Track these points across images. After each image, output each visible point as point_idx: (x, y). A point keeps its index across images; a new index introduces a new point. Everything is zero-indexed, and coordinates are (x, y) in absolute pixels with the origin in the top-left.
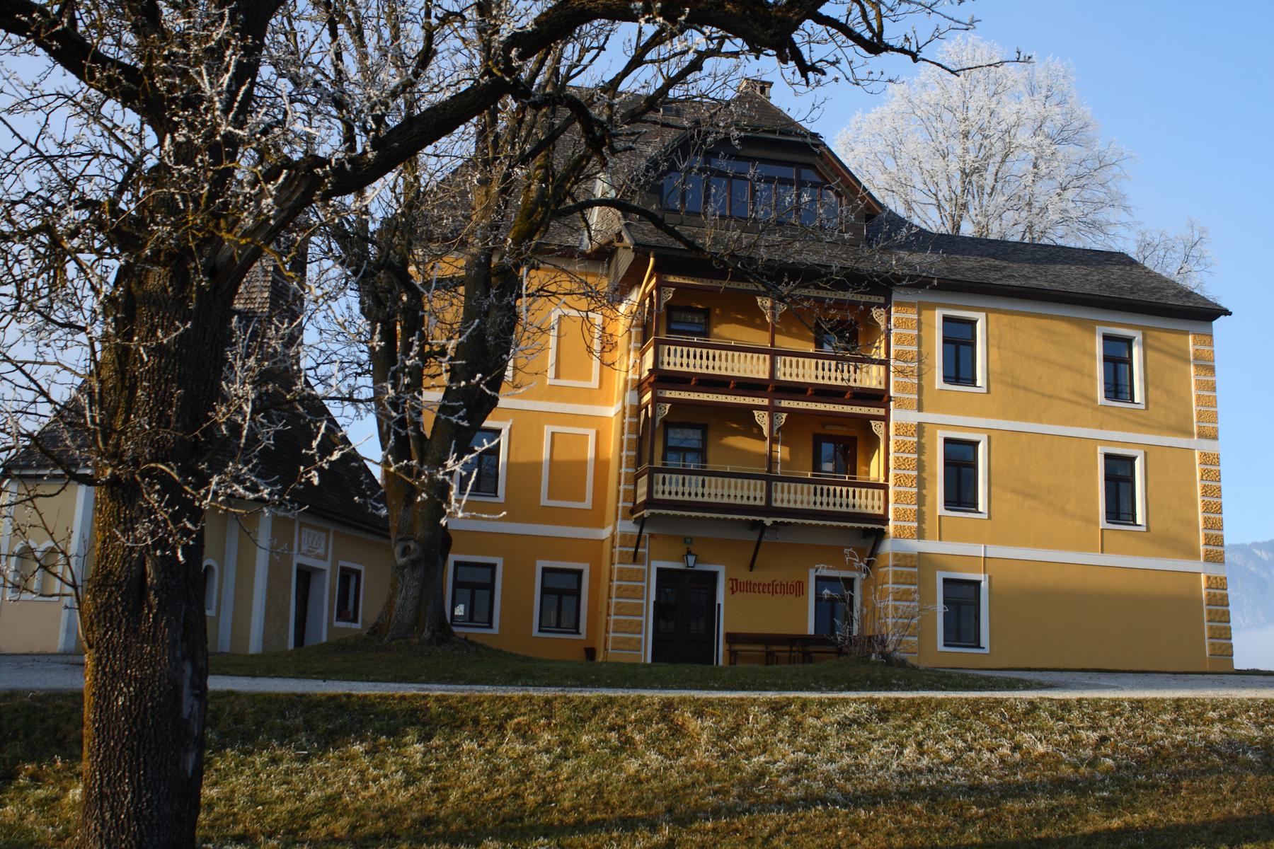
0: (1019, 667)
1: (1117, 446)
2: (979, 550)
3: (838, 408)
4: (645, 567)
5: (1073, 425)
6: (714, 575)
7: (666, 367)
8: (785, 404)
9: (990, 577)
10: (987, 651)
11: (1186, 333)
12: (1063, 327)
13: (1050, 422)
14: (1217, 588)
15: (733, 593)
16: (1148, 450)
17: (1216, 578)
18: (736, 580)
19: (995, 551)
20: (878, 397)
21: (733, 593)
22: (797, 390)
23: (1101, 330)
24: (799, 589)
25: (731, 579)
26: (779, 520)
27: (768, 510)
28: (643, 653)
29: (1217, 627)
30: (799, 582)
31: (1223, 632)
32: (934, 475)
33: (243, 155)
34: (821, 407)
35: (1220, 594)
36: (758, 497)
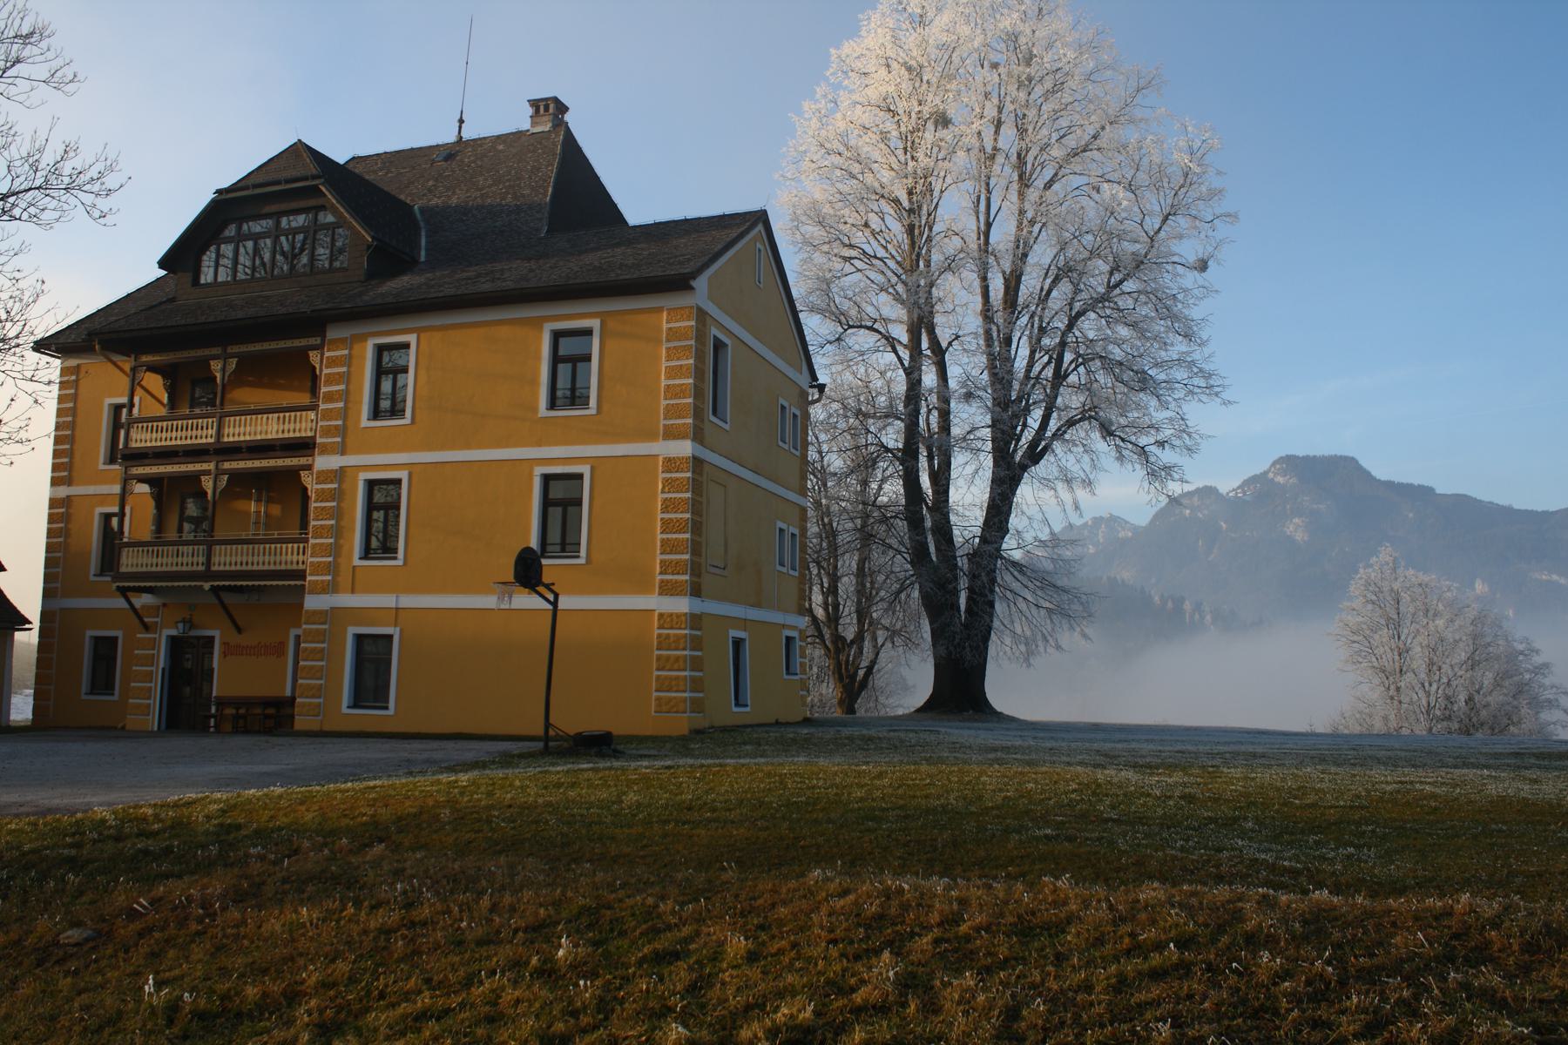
0: (424, 730)
1: (558, 465)
2: (387, 601)
3: (272, 463)
4: (157, 636)
5: (507, 446)
6: (212, 639)
7: (226, 440)
8: (227, 465)
9: (401, 631)
10: (391, 712)
11: (660, 310)
12: (504, 332)
13: (481, 446)
14: (672, 628)
15: (225, 656)
16: (596, 463)
17: (671, 615)
18: (228, 644)
19: (408, 601)
20: (304, 446)
21: (225, 656)
22: (235, 450)
23: (548, 328)
24: (280, 649)
25: (224, 643)
26: (216, 583)
27: (208, 575)
28: (151, 717)
29: (666, 677)
30: (281, 643)
31: (674, 683)
32: (353, 521)
33: (1034, 287)
34: (257, 464)
35: (675, 635)
36: (200, 562)
